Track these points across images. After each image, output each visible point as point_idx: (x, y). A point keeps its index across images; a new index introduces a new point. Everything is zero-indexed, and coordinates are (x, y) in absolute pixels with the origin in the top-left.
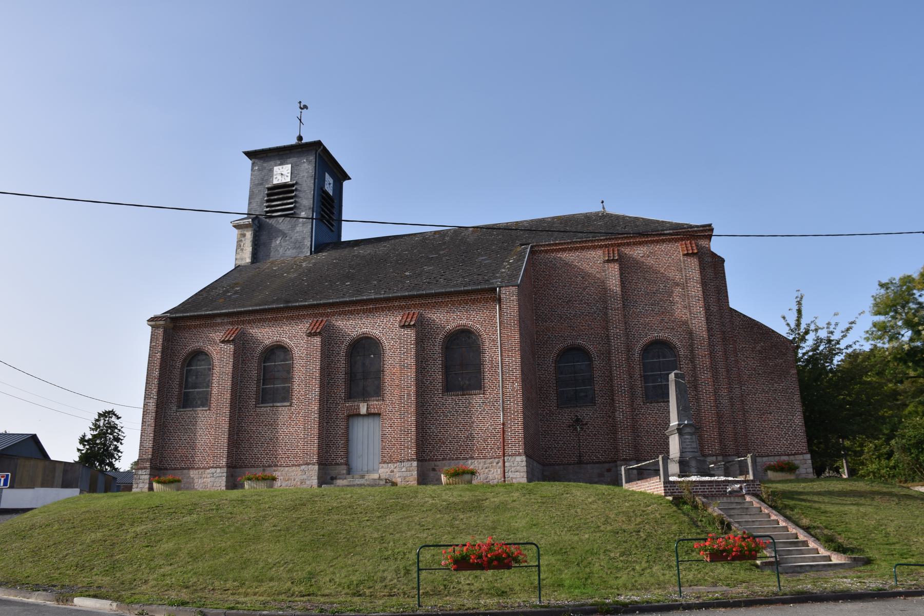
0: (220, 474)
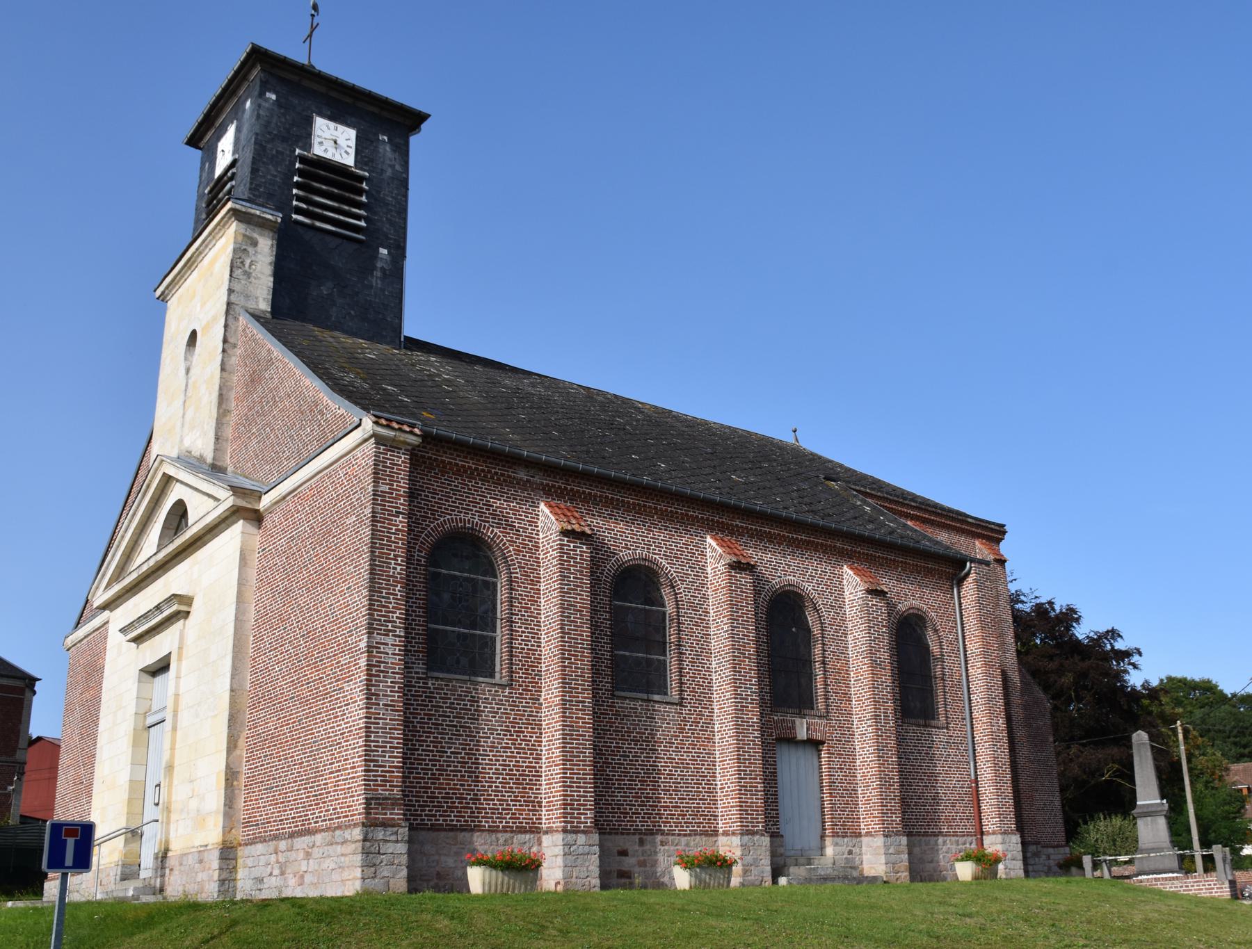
0: (587, 849)
